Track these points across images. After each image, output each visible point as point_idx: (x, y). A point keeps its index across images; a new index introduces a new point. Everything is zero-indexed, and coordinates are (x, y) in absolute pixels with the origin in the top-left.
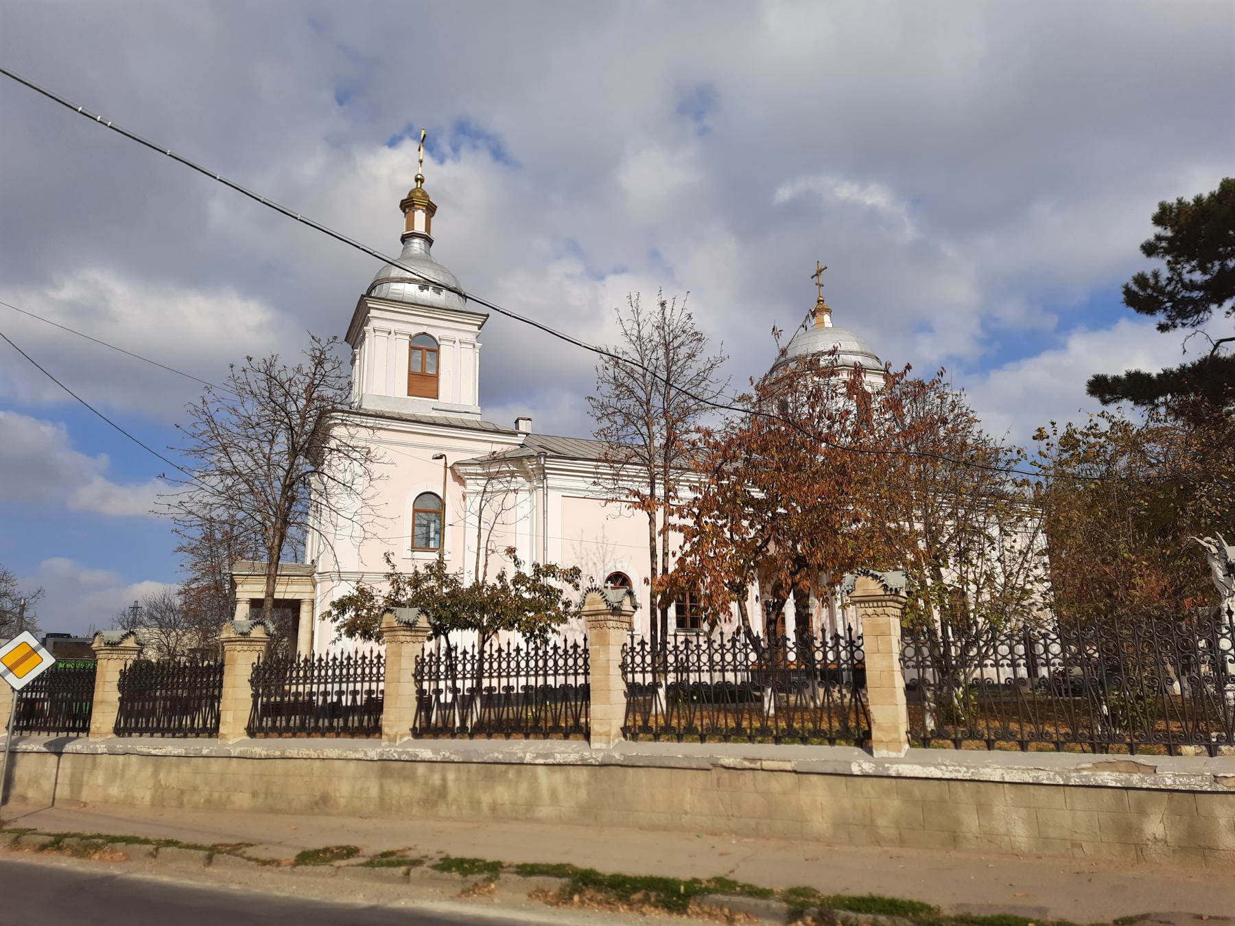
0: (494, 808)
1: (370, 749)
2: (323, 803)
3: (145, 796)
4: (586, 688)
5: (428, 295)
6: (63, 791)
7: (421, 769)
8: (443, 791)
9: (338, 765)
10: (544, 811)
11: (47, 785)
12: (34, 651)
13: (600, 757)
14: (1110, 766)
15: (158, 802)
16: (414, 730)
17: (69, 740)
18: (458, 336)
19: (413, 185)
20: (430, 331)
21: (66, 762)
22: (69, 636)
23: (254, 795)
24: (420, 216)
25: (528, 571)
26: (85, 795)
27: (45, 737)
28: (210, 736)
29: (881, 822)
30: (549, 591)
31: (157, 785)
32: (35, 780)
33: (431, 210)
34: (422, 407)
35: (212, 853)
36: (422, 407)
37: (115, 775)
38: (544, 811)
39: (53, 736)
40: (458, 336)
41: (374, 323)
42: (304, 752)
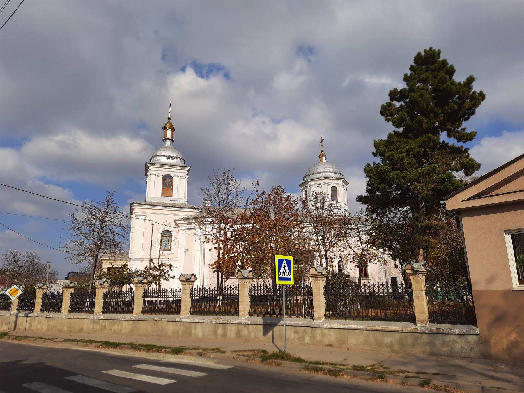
0: (114, 331)
1: (91, 316)
2: (81, 329)
3: (45, 328)
4: (180, 300)
5: (170, 161)
6: (28, 327)
7: (101, 321)
8: (104, 327)
9: (327, 331)
10: (123, 332)
11: (24, 325)
12: (17, 290)
13: (134, 318)
14: (213, 318)
15: (48, 330)
16: (190, 312)
17: (30, 313)
18: (180, 174)
19: (167, 121)
20: (170, 173)
21: (29, 319)
22: (78, 272)
23: (68, 328)
24: (169, 132)
25: (157, 265)
26: (33, 328)
27: (25, 312)
28: (177, 314)
29: (180, 332)
30: (162, 271)
31: (48, 326)
32: (22, 324)
33: (173, 130)
34: (166, 200)
35: (45, 340)
36: (166, 200)
37: (39, 322)
38: (123, 332)
39: (27, 312)
40: (180, 174)
41: (150, 172)
42: (78, 317)
